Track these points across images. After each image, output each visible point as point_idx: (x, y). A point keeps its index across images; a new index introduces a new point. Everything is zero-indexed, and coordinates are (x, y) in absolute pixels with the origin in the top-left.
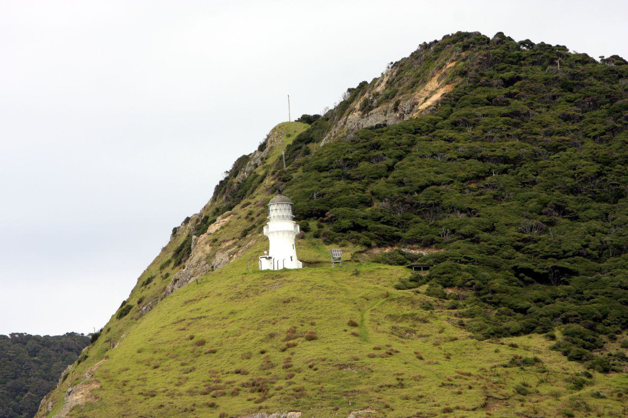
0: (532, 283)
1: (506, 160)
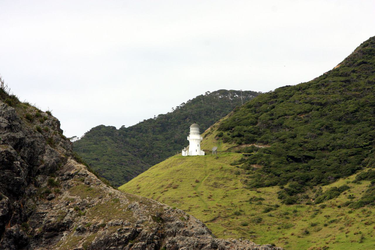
0: (292, 162)
1: (320, 104)
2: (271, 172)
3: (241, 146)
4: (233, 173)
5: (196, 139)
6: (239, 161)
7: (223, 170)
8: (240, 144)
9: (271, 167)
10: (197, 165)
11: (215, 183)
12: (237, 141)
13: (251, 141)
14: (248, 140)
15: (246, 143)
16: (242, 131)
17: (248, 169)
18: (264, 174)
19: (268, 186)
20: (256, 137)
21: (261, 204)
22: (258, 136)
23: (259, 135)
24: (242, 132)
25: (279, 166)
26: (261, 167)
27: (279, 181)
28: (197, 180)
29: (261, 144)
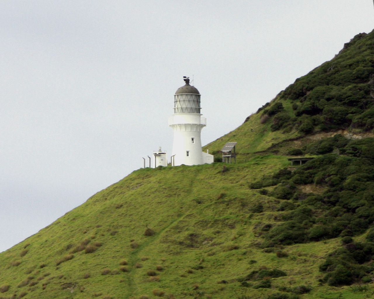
2: (338, 204)
3: (311, 138)
4: (246, 209)
5: (186, 125)
6: (274, 177)
7: (223, 202)
8: (308, 132)
9: (342, 189)
10: (166, 191)
11: (192, 235)
12: (302, 126)
13: (338, 124)
14: (331, 120)
15: (325, 130)
16: (323, 97)
17: (286, 196)
18: (319, 208)
19: (317, 238)
20: (352, 113)
21: (269, 286)
22: (359, 109)
23: (361, 107)
24: (322, 100)
25: (362, 187)
26: (321, 191)
27: (345, 226)
28: (148, 230)
29: (357, 130)
